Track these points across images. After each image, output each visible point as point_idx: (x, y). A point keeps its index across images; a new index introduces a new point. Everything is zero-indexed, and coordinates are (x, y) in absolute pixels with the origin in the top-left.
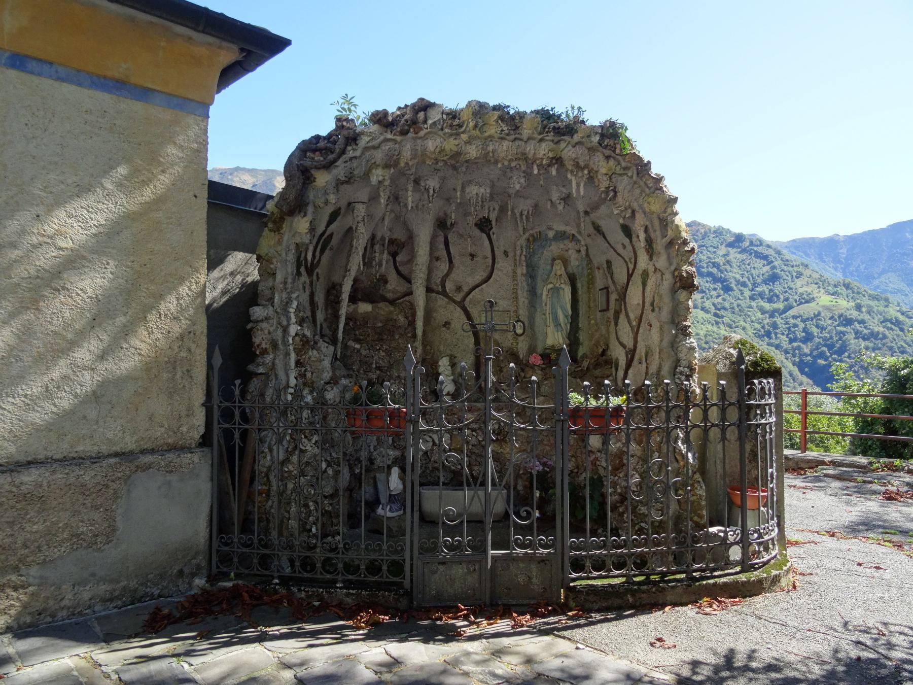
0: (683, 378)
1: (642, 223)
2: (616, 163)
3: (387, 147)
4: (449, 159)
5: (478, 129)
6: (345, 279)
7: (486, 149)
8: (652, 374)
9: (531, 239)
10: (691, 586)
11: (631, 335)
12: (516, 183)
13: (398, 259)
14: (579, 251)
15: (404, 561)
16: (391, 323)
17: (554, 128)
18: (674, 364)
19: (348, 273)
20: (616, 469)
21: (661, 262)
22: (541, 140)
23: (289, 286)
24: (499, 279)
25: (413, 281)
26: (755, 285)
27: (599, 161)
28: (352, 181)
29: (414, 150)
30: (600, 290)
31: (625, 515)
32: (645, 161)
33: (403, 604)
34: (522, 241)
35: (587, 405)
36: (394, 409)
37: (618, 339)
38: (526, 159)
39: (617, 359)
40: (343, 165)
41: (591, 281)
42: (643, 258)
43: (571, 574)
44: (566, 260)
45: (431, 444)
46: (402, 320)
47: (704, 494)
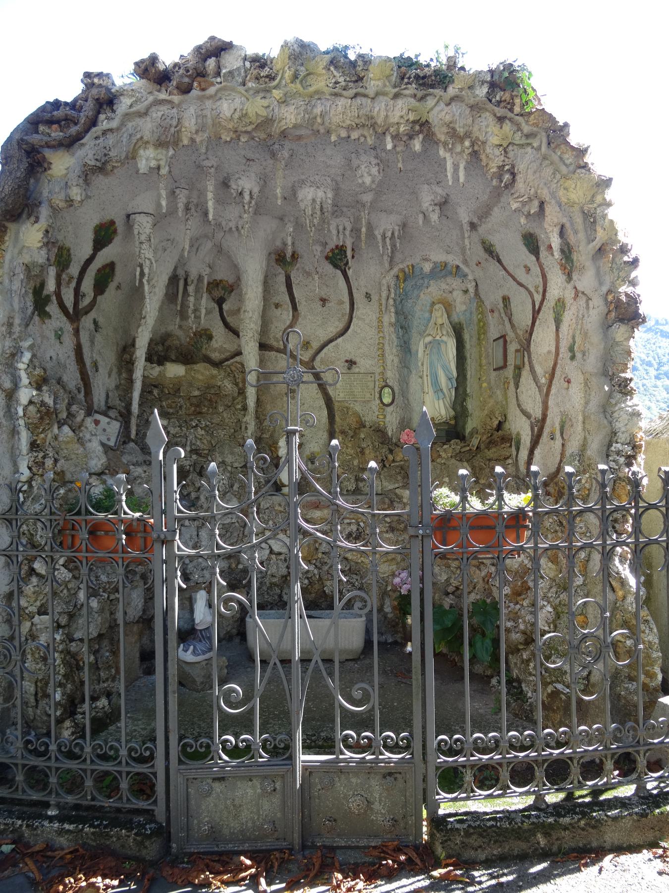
0: (622, 460)
1: (556, 220)
2: (515, 128)
3: (160, 114)
4: (255, 129)
5: (298, 81)
6: (140, 330)
7: (311, 113)
8: (572, 455)
9: (401, 275)
10: (647, 815)
11: (539, 399)
12: (366, 175)
13: (225, 307)
14: (466, 291)
15: (155, 774)
16: (213, 391)
17: (417, 77)
18: (607, 439)
19: (143, 321)
20: (518, 593)
21: (586, 281)
22: (396, 96)
23: (17, 329)
24: (359, 331)
25: (241, 334)
26: (660, 364)
27: (487, 126)
28: (109, 168)
29: (201, 116)
30: (494, 341)
31: (532, 665)
32: (561, 124)
33: (152, 850)
34: (389, 279)
35: (464, 508)
36: (132, 520)
37: (519, 406)
38: (374, 126)
39: (518, 434)
40: (93, 143)
41: (482, 329)
42: (556, 281)
43: (438, 794)
44: (450, 305)
45: (268, 552)
46: (228, 386)
47: (657, 641)
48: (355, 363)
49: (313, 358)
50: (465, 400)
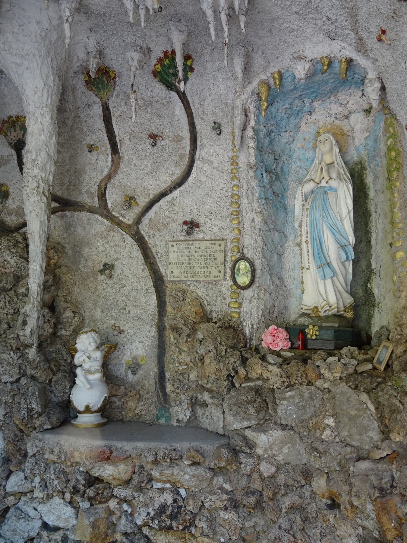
9: (264, 91)
24: (204, 179)
48: (197, 225)
49: (138, 220)
50: (369, 279)
